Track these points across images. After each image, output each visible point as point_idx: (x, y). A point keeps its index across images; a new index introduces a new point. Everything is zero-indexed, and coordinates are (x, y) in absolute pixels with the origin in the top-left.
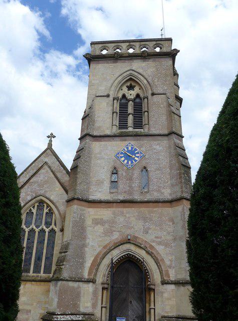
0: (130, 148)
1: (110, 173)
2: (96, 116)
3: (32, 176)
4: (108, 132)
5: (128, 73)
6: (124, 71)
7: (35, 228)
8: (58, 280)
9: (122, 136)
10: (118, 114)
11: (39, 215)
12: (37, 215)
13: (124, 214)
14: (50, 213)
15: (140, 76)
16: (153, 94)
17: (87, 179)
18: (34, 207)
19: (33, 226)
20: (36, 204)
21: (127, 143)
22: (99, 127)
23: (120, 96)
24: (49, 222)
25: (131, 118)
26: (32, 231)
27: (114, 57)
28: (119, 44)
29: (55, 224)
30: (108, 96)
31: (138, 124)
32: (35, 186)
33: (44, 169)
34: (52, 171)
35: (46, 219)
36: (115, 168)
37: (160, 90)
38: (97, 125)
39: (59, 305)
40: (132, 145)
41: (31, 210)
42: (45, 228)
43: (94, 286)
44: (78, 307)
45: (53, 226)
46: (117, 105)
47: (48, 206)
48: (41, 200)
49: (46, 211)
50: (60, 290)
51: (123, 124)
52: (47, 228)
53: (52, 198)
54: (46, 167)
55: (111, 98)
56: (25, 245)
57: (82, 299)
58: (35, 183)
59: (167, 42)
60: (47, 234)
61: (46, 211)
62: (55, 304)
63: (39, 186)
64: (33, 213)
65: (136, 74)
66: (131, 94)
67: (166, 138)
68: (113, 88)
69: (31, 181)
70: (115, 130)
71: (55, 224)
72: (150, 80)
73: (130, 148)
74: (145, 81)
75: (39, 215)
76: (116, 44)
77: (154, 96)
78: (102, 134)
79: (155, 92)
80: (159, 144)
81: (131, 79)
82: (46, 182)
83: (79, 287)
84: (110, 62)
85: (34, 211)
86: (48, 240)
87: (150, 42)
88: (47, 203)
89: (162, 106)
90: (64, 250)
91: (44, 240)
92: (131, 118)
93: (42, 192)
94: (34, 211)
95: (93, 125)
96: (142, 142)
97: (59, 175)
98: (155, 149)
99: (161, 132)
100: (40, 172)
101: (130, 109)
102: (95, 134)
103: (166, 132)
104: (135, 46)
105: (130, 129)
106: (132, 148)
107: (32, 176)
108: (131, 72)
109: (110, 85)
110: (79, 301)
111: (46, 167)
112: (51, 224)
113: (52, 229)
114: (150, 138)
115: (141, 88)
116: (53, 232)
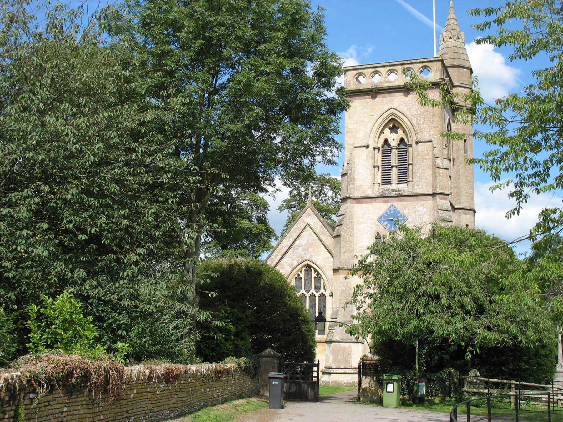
0: (392, 211)
1: (373, 168)
2: (356, 173)
3: (296, 240)
4: (370, 193)
5: (389, 112)
6: (385, 110)
7: (305, 293)
8: (330, 342)
9: (383, 197)
10: (380, 169)
11: (308, 279)
12: (305, 279)
13: (90, 318)
14: (319, 277)
15: (403, 117)
16: (417, 143)
17: (351, 247)
18: (301, 272)
19: (313, 291)
20: (304, 269)
21: (389, 204)
22: (360, 186)
23: (382, 142)
24: (318, 286)
25: (394, 171)
26: (313, 296)
27: (371, 91)
28: (377, 69)
29: (324, 289)
30: (367, 147)
31: (402, 180)
32: (300, 250)
33: (307, 231)
34: (315, 234)
35: (315, 284)
36: (378, 233)
37: (426, 137)
38: (357, 183)
39: (334, 361)
40: (395, 207)
41: (299, 274)
42: (315, 293)
43: (363, 345)
44: (351, 363)
45: (322, 290)
46: (379, 156)
47: (315, 270)
48: (308, 264)
49: (314, 275)
50: (334, 349)
51: (386, 180)
52: (317, 292)
53: (318, 263)
54: (308, 228)
55: (371, 148)
56: (307, 307)
57: (353, 356)
58: (299, 246)
59: (435, 63)
60: (317, 298)
61: (314, 275)
62: (331, 360)
63: (304, 249)
64: (301, 278)
65: (398, 114)
66: (394, 139)
67: (431, 197)
68: (372, 135)
69: (295, 244)
70: (376, 191)
71: (324, 289)
72: (414, 123)
73: (392, 211)
74: (409, 124)
75: (308, 279)
76: (374, 70)
77: (420, 144)
78: (363, 195)
79: (421, 138)
80: (422, 205)
81: (393, 119)
82: (311, 245)
83: (350, 347)
84: (367, 97)
85: (302, 275)
86: (319, 304)
87: (415, 65)
88: (314, 269)
89: (427, 157)
90: (334, 316)
91: (315, 304)
92: (394, 171)
93: (308, 257)
94: (302, 275)
95: (353, 184)
96: (405, 203)
97: (323, 238)
98: (418, 211)
99: (427, 193)
100: (303, 234)
101: (394, 160)
102: (357, 194)
103: (430, 191)
104: (397, 71)
105: (394, 186)
106: (395, 211)
107: (296, 240)
108: (392, 110)
109: (369, 131)
110: (351, 358)
111: (308, 228)
112: (320, 289)
113: (322, 293)
114: (416, 198)
115: (404, 131)
116: (322, 296)
